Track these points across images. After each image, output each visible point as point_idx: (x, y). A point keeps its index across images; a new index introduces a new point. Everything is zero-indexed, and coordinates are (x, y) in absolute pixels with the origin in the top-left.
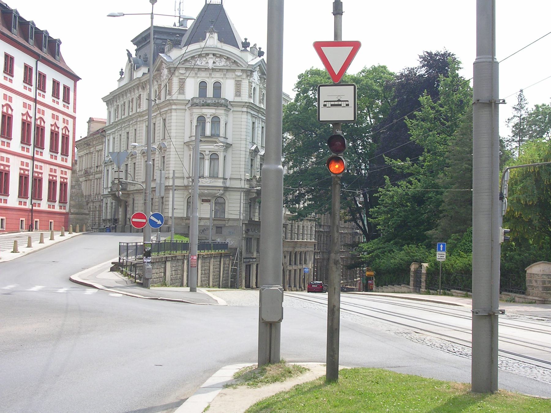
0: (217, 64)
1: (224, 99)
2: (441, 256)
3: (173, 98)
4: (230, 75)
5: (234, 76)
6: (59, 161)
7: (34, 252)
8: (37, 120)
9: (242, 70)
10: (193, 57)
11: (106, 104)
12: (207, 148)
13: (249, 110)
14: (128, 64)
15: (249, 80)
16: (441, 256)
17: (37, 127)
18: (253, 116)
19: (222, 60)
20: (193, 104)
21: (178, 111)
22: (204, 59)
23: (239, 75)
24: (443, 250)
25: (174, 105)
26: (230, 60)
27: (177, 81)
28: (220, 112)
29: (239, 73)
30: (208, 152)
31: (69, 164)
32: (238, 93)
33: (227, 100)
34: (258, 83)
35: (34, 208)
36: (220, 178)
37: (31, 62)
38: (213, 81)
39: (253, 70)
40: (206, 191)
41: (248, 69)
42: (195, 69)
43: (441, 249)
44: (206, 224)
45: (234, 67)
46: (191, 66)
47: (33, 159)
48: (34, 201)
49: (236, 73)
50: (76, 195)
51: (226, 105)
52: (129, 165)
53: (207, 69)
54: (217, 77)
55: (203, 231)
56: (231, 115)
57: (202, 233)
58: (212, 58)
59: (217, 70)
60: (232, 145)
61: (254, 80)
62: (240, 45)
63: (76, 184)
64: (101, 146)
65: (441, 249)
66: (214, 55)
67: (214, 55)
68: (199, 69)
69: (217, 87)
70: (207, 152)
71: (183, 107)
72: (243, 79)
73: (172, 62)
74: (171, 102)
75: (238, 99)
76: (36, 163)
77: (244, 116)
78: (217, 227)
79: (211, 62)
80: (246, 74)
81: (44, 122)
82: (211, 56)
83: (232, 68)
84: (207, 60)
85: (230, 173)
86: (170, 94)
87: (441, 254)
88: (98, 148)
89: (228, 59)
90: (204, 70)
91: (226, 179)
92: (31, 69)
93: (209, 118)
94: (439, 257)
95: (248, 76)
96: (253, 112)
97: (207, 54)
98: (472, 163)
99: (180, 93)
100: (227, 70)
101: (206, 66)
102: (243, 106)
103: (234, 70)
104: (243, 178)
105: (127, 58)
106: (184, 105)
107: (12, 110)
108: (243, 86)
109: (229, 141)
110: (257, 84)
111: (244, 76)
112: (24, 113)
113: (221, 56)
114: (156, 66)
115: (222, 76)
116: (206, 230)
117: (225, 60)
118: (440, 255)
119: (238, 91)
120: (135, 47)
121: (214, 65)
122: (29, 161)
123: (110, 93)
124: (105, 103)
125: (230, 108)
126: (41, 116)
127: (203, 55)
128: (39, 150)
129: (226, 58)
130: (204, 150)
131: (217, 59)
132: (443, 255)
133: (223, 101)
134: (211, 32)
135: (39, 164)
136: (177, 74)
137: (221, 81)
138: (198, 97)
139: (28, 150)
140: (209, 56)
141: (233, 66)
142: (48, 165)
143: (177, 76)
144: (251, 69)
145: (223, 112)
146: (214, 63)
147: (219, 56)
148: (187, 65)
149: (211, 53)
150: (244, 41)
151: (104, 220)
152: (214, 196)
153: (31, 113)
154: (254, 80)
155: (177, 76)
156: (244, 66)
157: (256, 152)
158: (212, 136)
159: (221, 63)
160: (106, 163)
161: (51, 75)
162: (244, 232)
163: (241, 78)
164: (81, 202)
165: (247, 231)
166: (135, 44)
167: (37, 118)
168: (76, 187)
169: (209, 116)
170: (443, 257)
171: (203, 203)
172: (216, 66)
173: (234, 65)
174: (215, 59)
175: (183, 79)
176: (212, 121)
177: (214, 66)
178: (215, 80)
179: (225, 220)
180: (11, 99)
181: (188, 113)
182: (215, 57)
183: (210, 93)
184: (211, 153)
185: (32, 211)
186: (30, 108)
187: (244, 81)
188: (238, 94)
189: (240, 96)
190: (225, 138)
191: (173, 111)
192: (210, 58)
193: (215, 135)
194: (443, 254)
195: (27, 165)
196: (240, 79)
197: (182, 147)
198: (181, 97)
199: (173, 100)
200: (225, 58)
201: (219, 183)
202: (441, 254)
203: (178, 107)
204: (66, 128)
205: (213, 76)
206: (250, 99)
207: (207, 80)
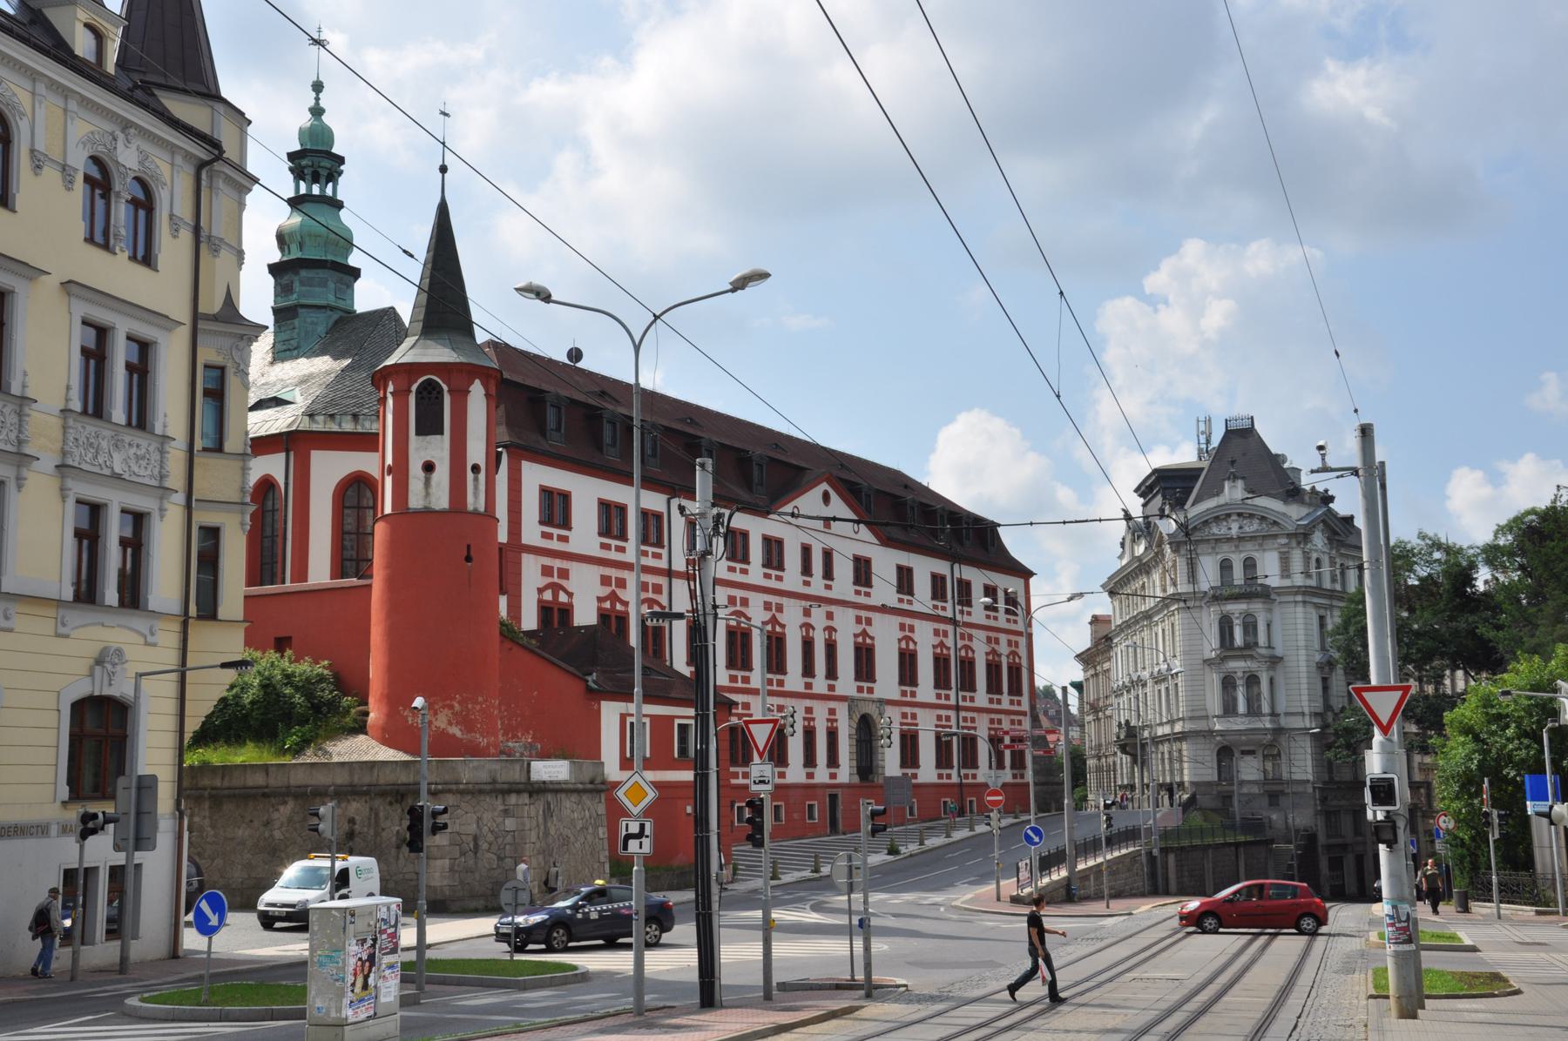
0: (1247, 529)
4: (1269, 543)
5: (1276, 546)
6: (1005, 705)
7: (953, 843)
8: (960, 650)
9: (1288, 534)
10: (1206, 523)
12: (1238, 666)
13: (1308, 599)
17: (961, 661)
18: (1317, 606)
20: (1216, 598)
28: (1257, 607)
29: (1284, 541)
31: (1025, 706)
32: (1285, 571)
34: (1325, 550)
35: (964, 781)
37: (942, 567)
38: (1243, 556)
45: (1275, 530)
47: (957, 708)
48: (963, 772)
49: (1279, 541)
51: (1265, 594)
52: (1180, 684)
53: (1230, 540)
54: (1250, 550)
56: (1277, 610)
60: (1282, 658)
64: (1108, 664)
66: (1239, 515)
67: (1239, 515)
68: (1216, 540)
69: (1250, 564)
76: (963, 714)
77: (1300, 609)
78: (1224, 797)
79: (1235, 528)
81: (973, 652)
85: (1284, 705)
88: (1106, 666)
91: (1279, 715)
92: (943, 578)
95: (1299, 543)
96: (1316, 600)
97: (1229, 515)
98: (763, 838)
100: (1263, 536)
102: (1296, 593)
103: (1275, 536)
104: (1306, 710)
107: (915, 643)
109: (1279, 652)
110: (1324, 552)
111: (1294, 543)
112: (936, 643)
113: (1251, 516)
120: (1142, 500)
122: (952, 714)
126: (967, 642)
128: (968, 694)
134: (1234, 478)
135: (969, 715)
137: (1256, 555)
139: (947, 697)
142: (985, 715)
146: (1241, 528)
151: (1120, 787)
153: (949, 642)
159: (1252, 527)
161: (977, 578)
162: (1318, 802)
165: (1324, 800)
166: (1140, 496)
167: (959, 646)
173: (1275, 528)
180: (912, 629)
183: (1238, 576)
185: (961, 785)
186: (945, 634)
190: (1270, 647)
192: (1233, 521)
193: (1250, 645)
195: (948, 718)
201: (1267, 723)
204: (1014, 654)
205: (1241, 548)
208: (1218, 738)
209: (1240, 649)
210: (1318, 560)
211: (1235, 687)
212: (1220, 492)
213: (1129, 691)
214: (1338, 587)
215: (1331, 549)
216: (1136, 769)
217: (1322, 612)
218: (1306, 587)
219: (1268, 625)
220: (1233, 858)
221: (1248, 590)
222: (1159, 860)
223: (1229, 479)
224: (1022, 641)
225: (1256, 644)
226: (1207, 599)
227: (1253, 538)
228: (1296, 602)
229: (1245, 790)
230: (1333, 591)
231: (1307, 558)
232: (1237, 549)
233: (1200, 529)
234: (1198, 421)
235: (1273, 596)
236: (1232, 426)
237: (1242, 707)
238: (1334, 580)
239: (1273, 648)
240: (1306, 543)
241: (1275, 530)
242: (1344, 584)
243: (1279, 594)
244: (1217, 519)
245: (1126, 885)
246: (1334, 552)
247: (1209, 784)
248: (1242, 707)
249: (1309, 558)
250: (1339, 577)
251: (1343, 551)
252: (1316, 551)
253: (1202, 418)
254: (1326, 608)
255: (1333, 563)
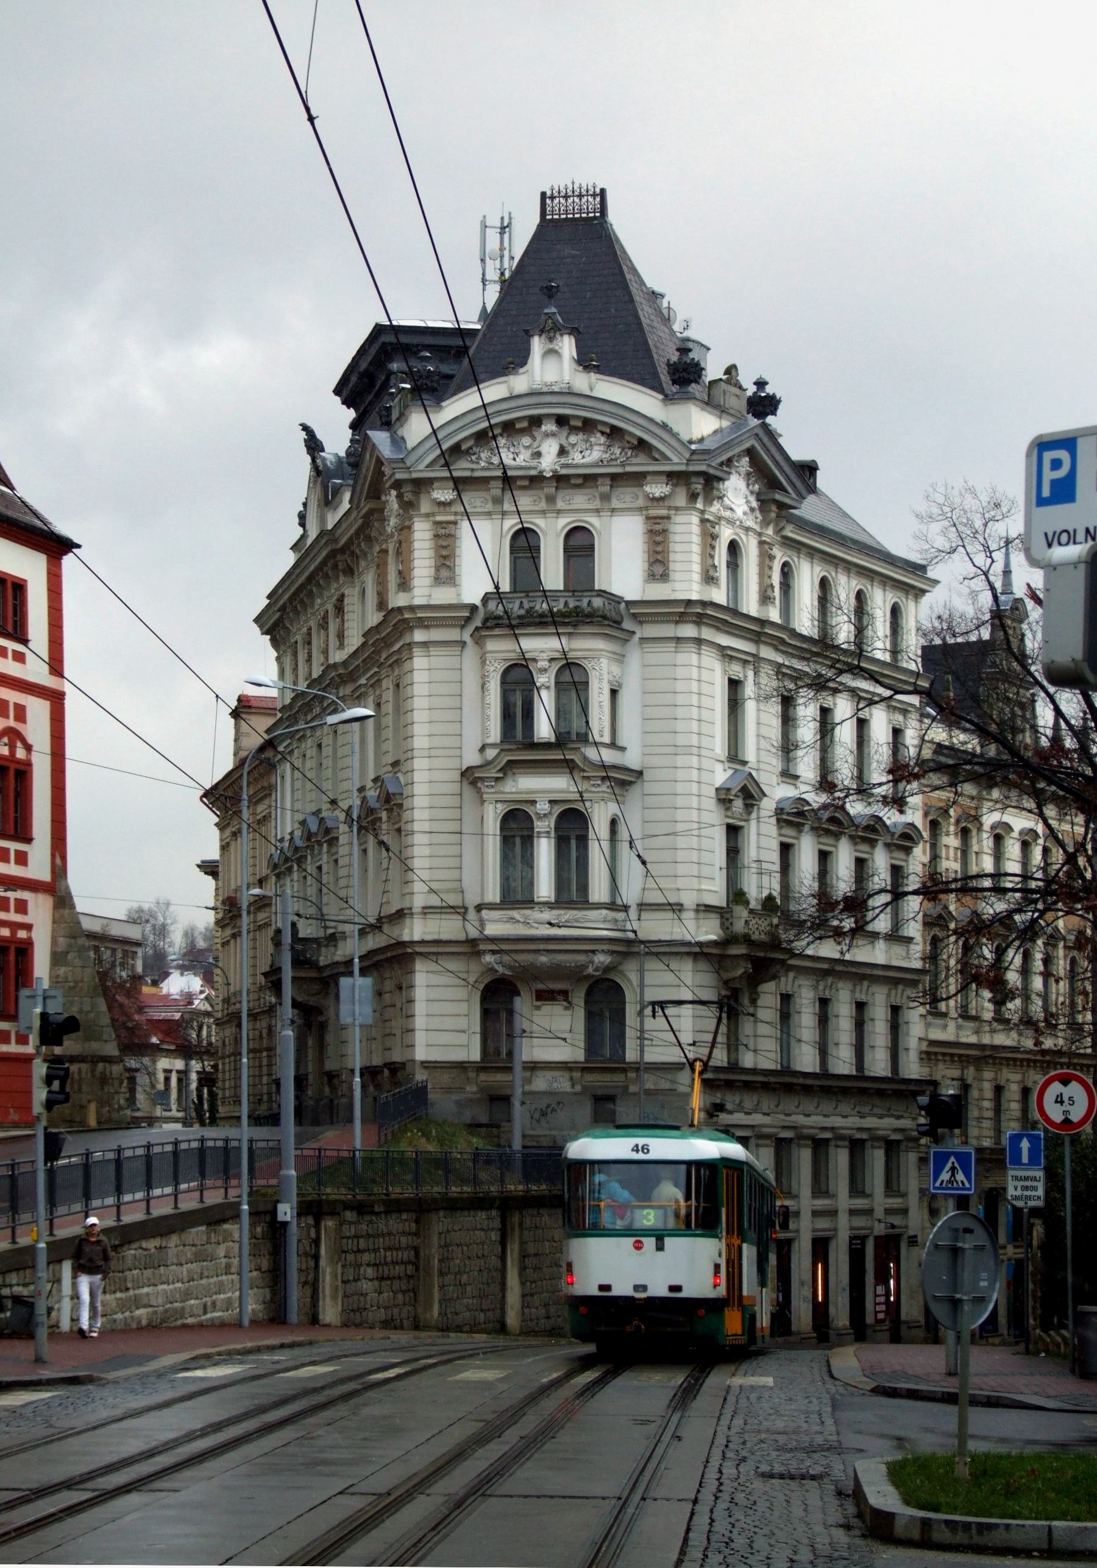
0: (576, 457)
1: (602, 593)
2: (1026, 1188)
3: (418, 601)
4: (624, 497)
5: (641, 502)
10: (482, 437)
11: (271, 640)
14: (315, 482)
15: (703, 512)
16: (1026, 1188)
18: (726, 654)
19: (592, 439)
21: (433, 651)
22: (526, 441)
23: (657, 495)
24: (1033, 1160)
25: (418, 627)
26: (623, 437)
27: (428, 535)
29: (658, 489)
30: (547, 806)
33: (616, 600)
34: (750, 523)
36: (598, 906)
38: (563, 523)
39: (711, 471)
40: (543, 959)
41: (691, 468)
42: (493, 484)
43: (1025, 1159)
44: (555, 1085)
45: (639, 464)
46: (473, 470)
49: (647, 489)
50: (71, 988)
53: (536, 481)
55: (544, 1114)
57: (538, 1121)
58: (553, 435)
59: (573, 481)
60: (640, 773)
61: (728, 514)
62: (665, 378)
63: (70, 946)
65: (1025, 1159)
66: (562, 421)
67: (562, 421)
70: (543, 807)
71: (453, 634)
72: (677, 509)
73: (402, 460)
74: (406, 616)
75: (658, 592)
79: (550, 449)
80: (688, 489)
82: (549, 427)
83: (628, 469)
84: (536, 444)
86: (405, 585)
87: (1026, 1179)
89: (615, 433)
90: (526, 483)
91: (625, 908)
93: (545, 670)
94: (1019, 1193)
95: (693, 497)
96: (725, 640)
97: (536, 421)
99: (438, 581)
100: (614, 477)
101: (530, 468)
103: (638, 478)
105: (309, 459)
106: (454, 626)
108: (677, 538)
109: (632, 759)
110: (747, 529)
111: (681, 500)
113: (588, 426)
114: (365, 477)
115: (543, 505)
116: (554, 1110)
117: (602, 439)
118: (1020, 1184)
119: (659, 557)
120: (351, 414)
121: (563, 460)
123: (269, 597)
124: (268, 637)
125: (632, 629)
127: (518, 426)
129: (608, 431)
130: (531, 797)
131: (573, 439)
132: (1035, 1184)
133: (597, 602)
134: (551, 331)
136: (425, 507)
137: (594, 522)
138: (561, 588)
140: (544, 428)
141: (635, 460)
143: (427, 515)
144: (703, 468)
145: (599, 644)
146: (562, 452)
147: (580, 424)
148: (462, 468)
149: (548, 416)
150: (674, 357)
152: (576, 975)
154: (728, 514)
155: (427, 515)
156: (675, 460)
157: (751, 796)
158: (562, 741)
160: (275, 866)
163: (669, 508)
164: (92, 1015)
168: (69, 957)
169: (545, 664)
170: (1035, 1188)
171: (539, 1003)
172: (567, 466)
173: (641, 458)
174: (567, 438)
175: (662, 518)
176: (556, 683)
177: (564, 466)
178: (569, 520)
179: (624, 1070)
181: (471, 653)
182: (565, 432)
184: (558, 810)
187: (679, 518)
188: (659, 570)
189: (664, 577)
190: (613, 745)
191: (417, 651)
192: (547, 435)
194: (1035, 1179)
196: (664, 512)
197: (456, 787)
198: (443, 596)
199: (412, 608)
200: (603, 433)
202: (1026, 1179)
203: (436, 635)
205: (560, 504)
206: (707, 587)
207: (539, 523)
208: (488, 958)
209: (546, 746)
210: (734, 547)
211: (528, 840)
212: (518, 359)
213: (300, 861)
214: (774, 614)
215: (765, 523)
216: (310, 1042)
217: (736, 671)
218: (704, 604)
219: (614, 693)
220: (494, 1236)
221: (572, 604)
222: (294, 1229)
223: (542, 332)
224: (38, 710)
225: (584, 738)
226: (478, 623)
227: (588, 480)
228: (678, 640)
229: (541, 1083)
230: (763, 622)
231: (709, 537)
232: (551, 508)
233: (468, 452)
234: (484, 227)
235: (627, 625)
236: (558, 209)
237: (545, 887)
238: (765, 599)
239: (623, 749)
240: (709, 501)
241: (639, 464)
242: (786, 609)
243: (638, 619)
244: (509, 428)
245: (186, 1295)
246: (770, 531)
247: (461, 1066)
248: (545, 887)
249: (714, 537)
250: (777, 592)
251: (789, 532)
252: (730, 522)
253: (494, 221)
254: (745, 662)
255: (766, 557)
